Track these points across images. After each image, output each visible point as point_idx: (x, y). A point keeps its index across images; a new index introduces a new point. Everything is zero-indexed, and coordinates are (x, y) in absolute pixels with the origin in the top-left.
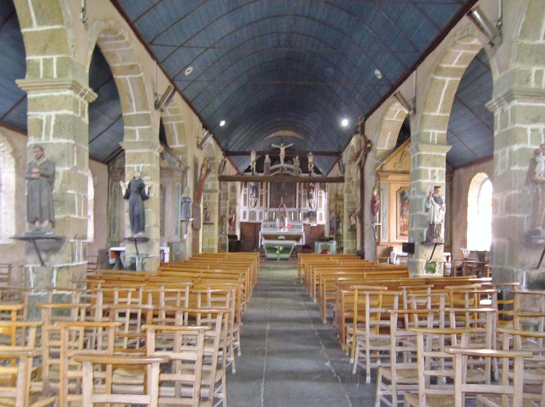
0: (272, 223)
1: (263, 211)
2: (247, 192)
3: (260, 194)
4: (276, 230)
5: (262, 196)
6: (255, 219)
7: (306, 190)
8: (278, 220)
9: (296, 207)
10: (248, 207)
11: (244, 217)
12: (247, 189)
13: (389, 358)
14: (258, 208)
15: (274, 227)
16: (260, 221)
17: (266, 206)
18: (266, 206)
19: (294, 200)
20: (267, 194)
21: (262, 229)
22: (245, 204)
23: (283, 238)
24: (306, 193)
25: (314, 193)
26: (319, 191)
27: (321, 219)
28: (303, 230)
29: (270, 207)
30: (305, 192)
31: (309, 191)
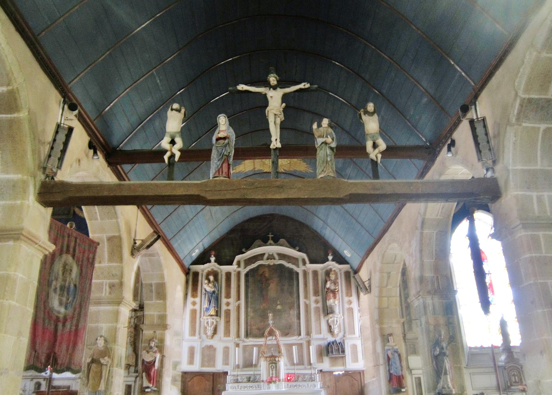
0: (250, 372)
1: (231, 345)
2: (197, 307)
3: (224, 308)
5: (228, 313)
6: (214, 366)
7: (320, 298)
9: (300, 335)
10: (200, 338)
11: (191, 361)
15: (255, 381)
17: (238, 336)
18: (238, 336)
19: (295, 320)
20: (239, 307)
22: (193, 332)
24: (320, 305)
25: (337, 302)
26: (346, 299)
27: (356, 360)
29: (247, 335)
30: (317, 302)
31: (325, 300)
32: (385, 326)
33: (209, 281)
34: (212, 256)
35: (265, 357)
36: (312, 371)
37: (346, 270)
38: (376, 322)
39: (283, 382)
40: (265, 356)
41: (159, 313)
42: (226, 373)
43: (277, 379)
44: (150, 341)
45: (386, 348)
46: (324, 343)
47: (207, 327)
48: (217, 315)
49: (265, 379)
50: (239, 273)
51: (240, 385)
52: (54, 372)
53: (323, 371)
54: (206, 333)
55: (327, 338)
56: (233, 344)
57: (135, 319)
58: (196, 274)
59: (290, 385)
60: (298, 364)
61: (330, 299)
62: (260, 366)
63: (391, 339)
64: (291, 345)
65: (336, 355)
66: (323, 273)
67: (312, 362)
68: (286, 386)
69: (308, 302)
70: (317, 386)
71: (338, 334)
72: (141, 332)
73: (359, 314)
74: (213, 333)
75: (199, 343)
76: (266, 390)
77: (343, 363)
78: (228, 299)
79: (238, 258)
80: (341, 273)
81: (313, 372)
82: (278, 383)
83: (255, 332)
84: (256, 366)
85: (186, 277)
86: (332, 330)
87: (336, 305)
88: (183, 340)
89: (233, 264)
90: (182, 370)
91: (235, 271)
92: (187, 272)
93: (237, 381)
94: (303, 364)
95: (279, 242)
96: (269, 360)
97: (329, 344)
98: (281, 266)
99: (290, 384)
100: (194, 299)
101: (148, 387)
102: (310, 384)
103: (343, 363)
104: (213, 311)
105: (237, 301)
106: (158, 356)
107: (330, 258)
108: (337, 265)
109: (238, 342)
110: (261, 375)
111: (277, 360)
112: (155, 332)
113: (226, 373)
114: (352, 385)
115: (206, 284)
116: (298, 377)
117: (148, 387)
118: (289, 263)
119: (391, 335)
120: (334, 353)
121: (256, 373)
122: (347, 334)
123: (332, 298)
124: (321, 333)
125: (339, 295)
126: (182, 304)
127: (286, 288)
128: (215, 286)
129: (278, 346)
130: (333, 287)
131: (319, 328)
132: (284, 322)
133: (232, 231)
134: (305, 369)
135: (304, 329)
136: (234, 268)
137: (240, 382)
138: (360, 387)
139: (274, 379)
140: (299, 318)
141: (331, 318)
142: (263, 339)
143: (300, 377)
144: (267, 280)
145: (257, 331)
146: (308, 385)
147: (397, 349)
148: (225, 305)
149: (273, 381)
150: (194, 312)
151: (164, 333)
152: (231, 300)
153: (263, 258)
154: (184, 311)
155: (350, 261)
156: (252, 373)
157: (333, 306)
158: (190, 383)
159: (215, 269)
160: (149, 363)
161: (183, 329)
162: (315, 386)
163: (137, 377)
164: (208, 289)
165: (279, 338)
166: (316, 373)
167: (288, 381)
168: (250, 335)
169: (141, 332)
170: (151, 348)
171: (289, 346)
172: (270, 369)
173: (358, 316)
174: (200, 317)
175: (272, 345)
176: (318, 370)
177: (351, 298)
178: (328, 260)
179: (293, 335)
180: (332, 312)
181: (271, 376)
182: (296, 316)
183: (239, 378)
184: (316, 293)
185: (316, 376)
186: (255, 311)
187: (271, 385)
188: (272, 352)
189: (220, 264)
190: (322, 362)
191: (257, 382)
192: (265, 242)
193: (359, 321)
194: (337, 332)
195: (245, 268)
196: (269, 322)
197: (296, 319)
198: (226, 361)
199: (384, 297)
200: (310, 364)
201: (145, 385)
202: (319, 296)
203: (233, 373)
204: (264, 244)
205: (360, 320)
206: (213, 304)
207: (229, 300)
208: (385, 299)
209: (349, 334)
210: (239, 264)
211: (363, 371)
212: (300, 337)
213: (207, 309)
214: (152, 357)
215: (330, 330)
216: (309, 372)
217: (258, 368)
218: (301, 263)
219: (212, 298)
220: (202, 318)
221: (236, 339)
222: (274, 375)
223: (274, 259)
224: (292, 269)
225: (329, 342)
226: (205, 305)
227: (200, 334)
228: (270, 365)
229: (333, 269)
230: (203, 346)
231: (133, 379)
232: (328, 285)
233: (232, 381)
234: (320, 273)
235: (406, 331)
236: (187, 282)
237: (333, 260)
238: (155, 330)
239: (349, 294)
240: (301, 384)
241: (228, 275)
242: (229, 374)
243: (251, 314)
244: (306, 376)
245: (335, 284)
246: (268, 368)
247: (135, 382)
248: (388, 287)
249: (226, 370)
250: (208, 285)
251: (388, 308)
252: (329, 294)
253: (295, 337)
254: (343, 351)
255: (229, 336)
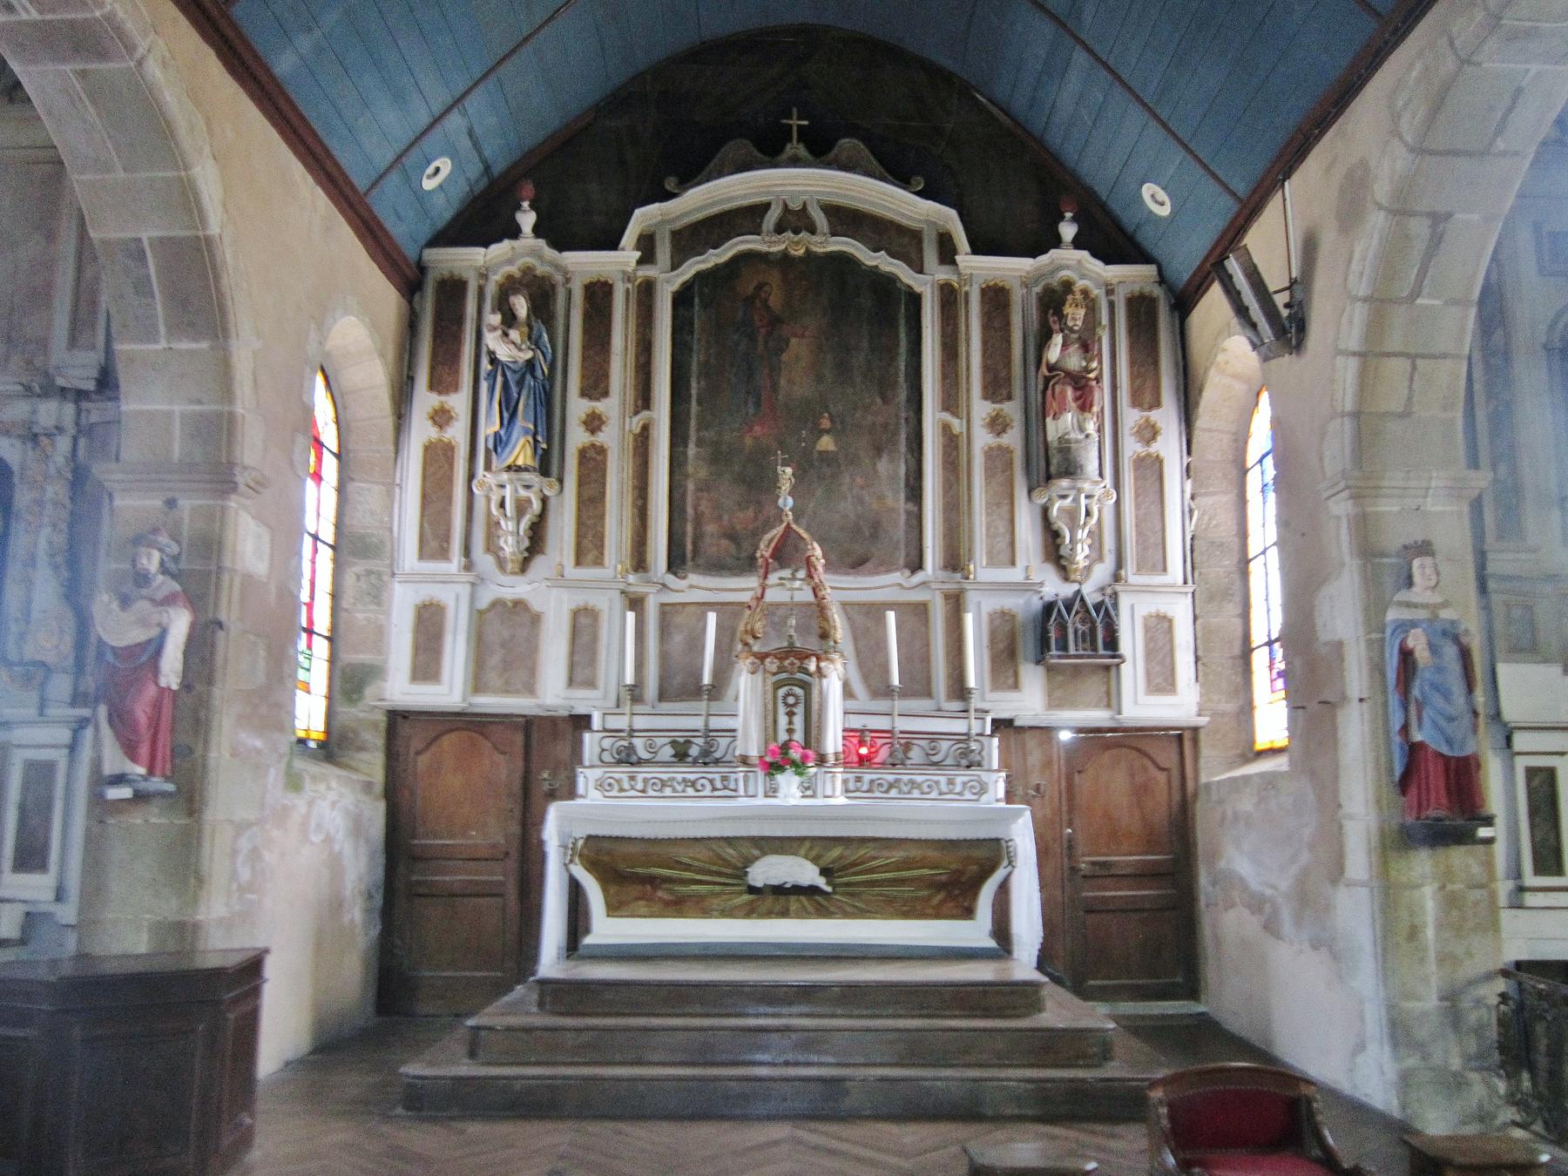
0: (687, 718)
1: (607, 603)
2: (457, 433)
3: (577, 438)
4: (726, 788)
5: (593, 460)
6: (530, 688)
7: (1012, 409)
8: (747, 686)
9: (916, 565)
10: (469, 567)
11: (426, 665)
12: (459, 402)
13: (844, 731)
14: (559, 580)
15: (707, 758)
16: (581, 701)
17: (640, 562)
18: (640, 562)
19: (901, 504)
20: (643, 441)
21: (587, 778)
22: (434, 543)
23: (805, 872)
24: (1013, 438)
25: (1091, 427)
26: (1131, 417)
27: (1162, 680)
28: (998, 785)
29: (676, 563)
30: (997, 425)
31: (1035, 419)
32: (1387, 507)
33: (510, 319)
34: (526, 204)
35: (755, 655)
36: (974, 722)
37: (1136, 289)
38: (1342, 485)
39: (835, 765)
40: (756, 648)
41: (198, 408)
42: (581, 722)
43: (810, 753)
44: (137, 541)
45: (1392, 615)
46: (1024, 606)
47: (502, 523)
48: (544, 470)
49: (754, 752)
50: (647, 291)
51: (643, 773)
52: (590, 728)
53: (1017, 723)
54: (492, 547)
55: (1041, 584)
56: (616, 595)
57: (75, 440)
58: (452, 290)
59: (872, 781)
60: (905, 693)
61: (1062, 409)
62: (736, 699)
63: (1422, 566)
64: (874, 611)
65: (1081, 657)
66: (1034, 301)
67: (971, 682)
68: (851, 786)
69: (957, 425)
70: (991, 787)
71: (1088, 569)
72: (106, 501)
73: (1189, 485)
74: (527, 550)
75: (465, 591)
76: (761, 801)
77: (1108, 693)
78: (598, 399)
79: (644, 217)
80: (1112, 305)
81: (976, 727)
82: (813, 770)
83: (715, 545)
84: (717, 690)
85: (410, 302)
86: (1064, 551)
87: (1087, 436)
88: (393, 574)
89: (623, 242)
90: (387, 705)
91: (628, 278)
92: (410, 279)
93: (627, 758)
94: (928, 694)
95: (835, 151)
96: (774, 668)
97: (1049, 608)
98: (843, 262)
99: (868, 776)
100: (443, 398)
101: (119, 780)
102: (959, 780)
103: (1108, 693)
104: (529, 451)
105: (636, 413)
106: (180, 624)
107: (1068, 231)
108: (1096, 266)
109: (642, 589)
110: (739, 734)
111: (812, 667)
112: (171, 503)
113: (581, 722)
114: (1141, 791)
115: (494, 329)
116: (907, 747)
117: (119, 780)
118: (876, 250)
119: (1424, 549)
120: (1072, 651)
121: (715, 723)
122: (1129, 571)
123: (1073, 405)
124: (1013, 563)
125: (1102, 397)
126: (388, 422)
127: (859, 359)
128: (536, 343)
129: (819, 608)
130: (1074, 362)
131: (1008, 537)
132: (847, 507)
133: (619, 101)
134: (939, 713)
135: (940, 543)
136: (627, 264)
137: (640, 762)
138: (1177, 797)
139: (795, 754)
140: (915, 492)
141: (1064, 497)
142: (752, 581)
143: (915, 748)
144: (775, 321)
145: (725, 543)
146: (951, 782)
147: (1453, 622)
148: (582, 429)
149: (793, 763)
150: (439, 456)
151: (224, 510)
152: (610, 406)
153: (760, 225)
154: (397, 452)
155: (1157, 253)
156: (698, 723)
157: (1077, 441)
158: (423, 761)
159: (541, 270)
160: (131, 652)
161: (395, 529)
162: (983, 789)
163: (82, 723)
164: (504, 353)
165: (828, 580)
166: (988, 732)
167: (863, 761)
168: (693, 559)
169: (106, 501)
170: (142, 579)
171: (868, 615)
172: (782, 710)
173: (1183, 492)
174: (471, 476)
175: (792, 606)
176: (994, 721)
177: (1154, 415)
178: (1057, 242)
179: (887, 566)
180: (1071, 469)
181: (783, 737)
182: (902, 484)
183: (639, 743)
184: (996, 387)
185: (986, 743)
186: (718, 457)
187: (780, 778)
188: (792, 632)
189: (561, 245)
190: (1016, 686)
191: (717, 762)
192: (770, 151)
193: (1187, 516)
194: (1086, 557)
195: (674, 267)
196: (781, 502)
197: (902, 496)
198: (581, 669)
199: (1394, 355)
200: (960, 690)
201: (108, 769)
202: (1009, 398)
203: (614, 723)
204: (767, 159)
205: (1191, 511)
206: (523, 422)
207: (600, 406)
208: (1399, 366)
209: (1140, 569)
210: (647, 246)
211: (1195, 730)
212: (919, 577)
213: (499, 442)
214: (144, 622)
215: (1054, 549)
216: (959, 726)
217: (723, 706)
218: (930, 255)
219: (524, 393)
220: (482, 484)
221: (632, 578)
222: (799, 736)
223: (812, 230)
224: (891, 280)
225: (1048, 598)
226: (489, 427)
227: (467, 551)
228: (782, 692)
229: (1081, 284)
230: (483, 603)
231: (64, 735)
232: (1053, 353)
233: (607, 757)
234: (1017, 296)
235: (1490, 538)
236: (411, 326)
237: (1078, 244)
238: (170, 495)
239: (1146, 397)
240: (919, 779)
241: (598, 295)
242: (596, 723)
243: (697, 469)
244: (945, 745)
245: (1086, 348)
246: (770, 707)
247: (73, 748)
248: (1419, 301)
249: (581, 710)
250: (506, 334)
251: (1405, 414)
252: (1058, 388)
253: (896, 577)
254: (1112, 643)
255: (599, 562)
